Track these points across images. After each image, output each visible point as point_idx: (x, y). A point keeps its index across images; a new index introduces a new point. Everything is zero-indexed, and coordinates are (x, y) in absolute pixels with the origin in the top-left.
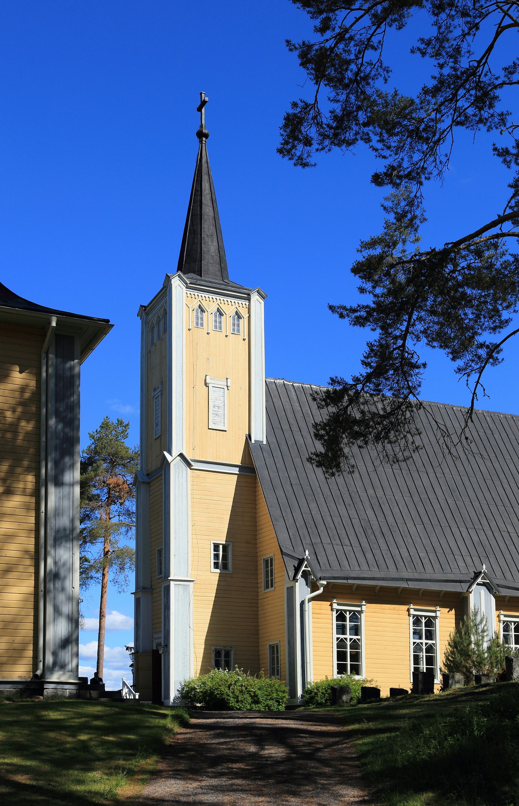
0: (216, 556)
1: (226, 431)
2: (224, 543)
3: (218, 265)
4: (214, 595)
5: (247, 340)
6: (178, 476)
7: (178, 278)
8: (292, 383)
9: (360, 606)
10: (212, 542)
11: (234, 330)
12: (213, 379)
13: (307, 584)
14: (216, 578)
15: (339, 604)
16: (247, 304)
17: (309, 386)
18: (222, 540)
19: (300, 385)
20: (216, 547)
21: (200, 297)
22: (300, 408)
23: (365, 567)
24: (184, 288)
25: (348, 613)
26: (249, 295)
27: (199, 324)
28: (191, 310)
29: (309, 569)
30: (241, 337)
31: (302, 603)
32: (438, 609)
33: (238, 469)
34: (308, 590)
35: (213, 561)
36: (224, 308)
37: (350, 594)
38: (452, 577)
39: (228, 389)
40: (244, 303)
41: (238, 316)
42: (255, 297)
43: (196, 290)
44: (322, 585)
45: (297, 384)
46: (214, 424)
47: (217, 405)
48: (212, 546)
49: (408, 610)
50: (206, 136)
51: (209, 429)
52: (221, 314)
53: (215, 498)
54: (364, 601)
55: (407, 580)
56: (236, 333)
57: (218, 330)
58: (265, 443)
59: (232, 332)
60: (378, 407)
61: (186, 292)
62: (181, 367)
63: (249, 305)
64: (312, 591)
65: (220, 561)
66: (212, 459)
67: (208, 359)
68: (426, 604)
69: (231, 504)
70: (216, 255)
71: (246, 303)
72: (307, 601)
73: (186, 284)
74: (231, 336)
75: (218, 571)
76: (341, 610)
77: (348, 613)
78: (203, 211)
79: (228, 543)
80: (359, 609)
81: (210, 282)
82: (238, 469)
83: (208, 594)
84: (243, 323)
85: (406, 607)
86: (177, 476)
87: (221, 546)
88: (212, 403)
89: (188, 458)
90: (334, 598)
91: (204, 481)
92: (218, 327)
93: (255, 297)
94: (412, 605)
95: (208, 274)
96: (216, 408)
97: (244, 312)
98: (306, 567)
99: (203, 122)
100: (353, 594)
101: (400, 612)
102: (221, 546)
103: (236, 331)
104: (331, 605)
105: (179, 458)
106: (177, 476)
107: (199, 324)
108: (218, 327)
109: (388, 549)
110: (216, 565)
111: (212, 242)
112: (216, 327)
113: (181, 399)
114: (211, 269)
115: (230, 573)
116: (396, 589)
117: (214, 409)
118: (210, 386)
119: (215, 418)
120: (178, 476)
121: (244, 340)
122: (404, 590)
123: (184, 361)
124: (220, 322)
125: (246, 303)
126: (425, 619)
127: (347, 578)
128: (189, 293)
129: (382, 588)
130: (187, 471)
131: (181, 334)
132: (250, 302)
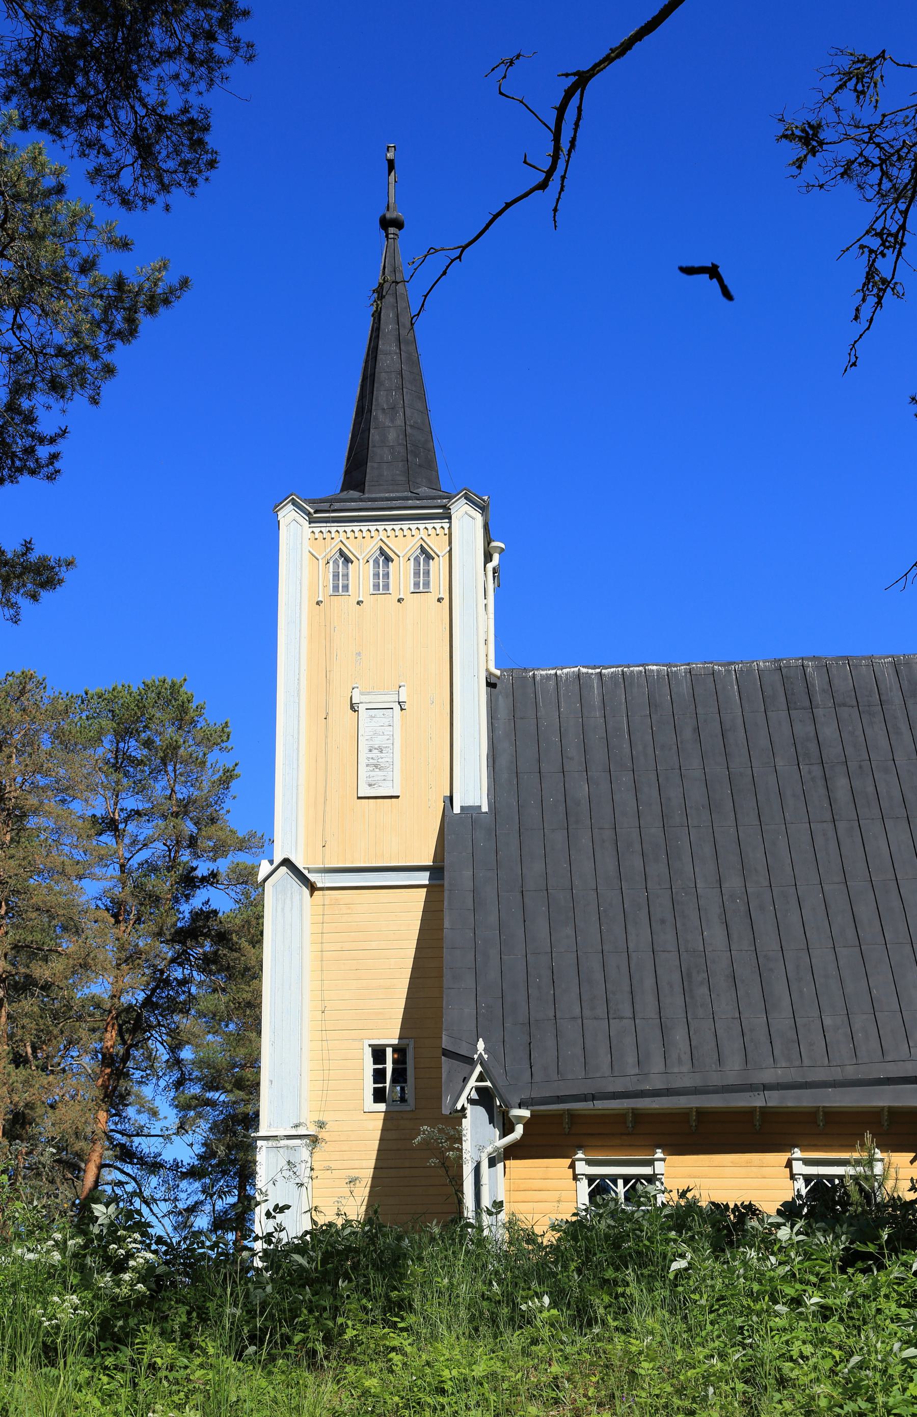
0: (379, 1075)
1: (398, 797)
2: (396, 1042)
3: (401, 464)
4: (372, 1163)
5: (446, 601)
6: (283, 909)
7: (292, 507)
8: (598, 670)
9: (650, 1163)
10: (367, 1042)
11: (417, 585)
12: (369, 693)
13: (491, 1121)
14: (377, 1123)
15: (590, 1163)
16: (446, 526)
17: (641, 668)
18: (390, 1036)
19: (620, 669)
20: (378, 1054)
21: (342, 534)
22: (602, 720)
23: (657, 1065)
24: (306, 524)
25: (620, 1182)
26: (446, 508)
27: (340, 586)
28: (322, 563)
29: (488, 1084)
30: (433, 597)
31: (477, 1170)
32: (659, 1154)
33: (427, 874)
34: (495, 1135)
35: (369, 1086)
36: (353, 548)
37: (622, 1134)
38: (851, 1072)
39: (402, 709)
40: (438, 526)
41: (426, 554)
42: (462, 510)
43: (333, 522)
44: (519, 1119)
45: (613, 670)
46: (370, 785)
47: (376, 746)
48: (369, 1051)
49: (789, 1165)
50: (399, 224)
51: (359, 798)
52: (388, 559)
53: (374, 945)
54: (659, 1151)
55: (765, 1087)
56: (421, 589)
57: (381, 592)
58: (485, 809)
59: (412, 590)
60: (814, 685)
61: (311, 529)
62: (296, 681)
63: (450, 528)
64: (504, 1134)
65: (388, 1085)
66: (365, 862)
67: (359, 654)
68: (842, 1146)
69: (412, 953)
70: (400, 445)
71: (444, 525)
72: (485, 1164)
73: (309, 514)
74: (410, 600)
75: (382, 1107)
76: (603, 1177)
77: (620, 1182)
78: (379, 364)
79: (405, 1041)
80: (647, 1170)
81: (388, 499)
82: (427, 874)
83: (356, 1164)
84: (438, 568)
85: (783, 1157)
86: (279, 909)
87: (389, 1051)
88: (367, 742)
89: (300, 867)
90: (580, 1147)
91: (349, 912)
92: (382, 585)
93: (462, 510)
94: (796, 1150)
95: (380, 485)
96: (376, 751)
97: (437, 545)
98: (481, 1078)
99: (392, 200)
100: (628, 1134)
101: (766, 1171)
102: (389, 1051)
103: (422, 584)
104: (572, 1166)
105: (283, 869)
106: (279, 909)
107: (340, 586)
108: (382, 585)
109: (737, 1015)
110: (379, 1095)
111: (392, 420)
112: (376, 586)
113: (295, 746)
114: (385, 474)
115: (408, 1108)
116: (749, 1113)
117: (370, 755)
118: (362, 708)
119: (372, 774)
120: (283, 909)
121: (439, 600)
122: (766, 1113)
123: (304, 666)
124: (387, 575)
125: (444, 525)
126: (625, 1185)
127: (594, 1098)
128: (317, 530)
129: (702, 1113)
130: (301, 894)
131: (298, 615)
132: (450, 523)
